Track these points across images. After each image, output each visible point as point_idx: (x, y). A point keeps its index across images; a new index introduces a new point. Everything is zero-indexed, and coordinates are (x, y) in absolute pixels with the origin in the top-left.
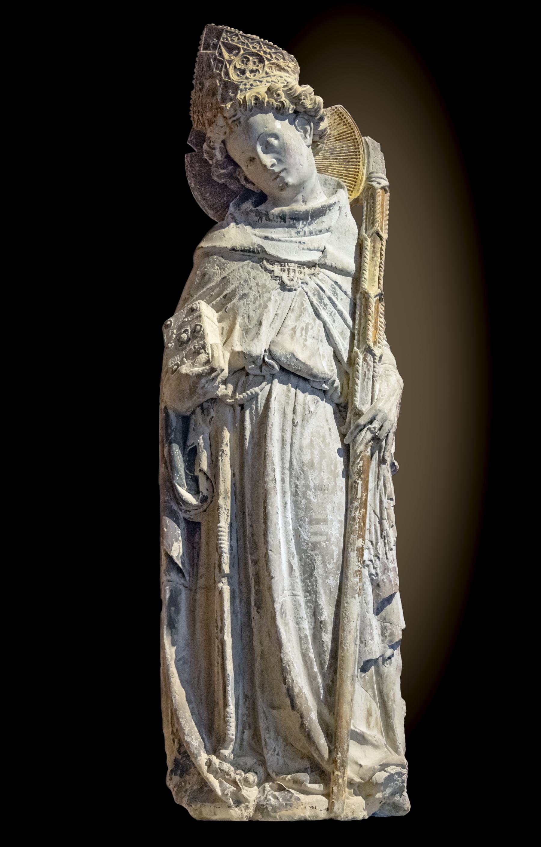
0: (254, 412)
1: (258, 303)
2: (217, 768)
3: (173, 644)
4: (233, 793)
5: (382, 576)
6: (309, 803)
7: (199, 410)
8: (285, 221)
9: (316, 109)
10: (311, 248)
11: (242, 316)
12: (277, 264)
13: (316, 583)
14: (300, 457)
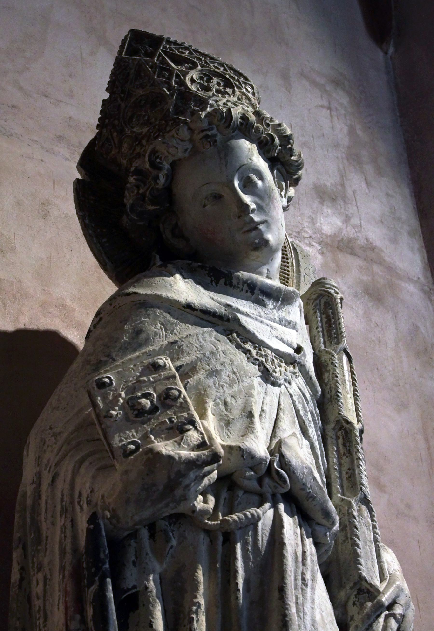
0: (250, 548)
1: (236, 388)
7: (145, 533)
8: (253, 293)
9: (300, 165)
10: (285, 339)
12: (251, 344)
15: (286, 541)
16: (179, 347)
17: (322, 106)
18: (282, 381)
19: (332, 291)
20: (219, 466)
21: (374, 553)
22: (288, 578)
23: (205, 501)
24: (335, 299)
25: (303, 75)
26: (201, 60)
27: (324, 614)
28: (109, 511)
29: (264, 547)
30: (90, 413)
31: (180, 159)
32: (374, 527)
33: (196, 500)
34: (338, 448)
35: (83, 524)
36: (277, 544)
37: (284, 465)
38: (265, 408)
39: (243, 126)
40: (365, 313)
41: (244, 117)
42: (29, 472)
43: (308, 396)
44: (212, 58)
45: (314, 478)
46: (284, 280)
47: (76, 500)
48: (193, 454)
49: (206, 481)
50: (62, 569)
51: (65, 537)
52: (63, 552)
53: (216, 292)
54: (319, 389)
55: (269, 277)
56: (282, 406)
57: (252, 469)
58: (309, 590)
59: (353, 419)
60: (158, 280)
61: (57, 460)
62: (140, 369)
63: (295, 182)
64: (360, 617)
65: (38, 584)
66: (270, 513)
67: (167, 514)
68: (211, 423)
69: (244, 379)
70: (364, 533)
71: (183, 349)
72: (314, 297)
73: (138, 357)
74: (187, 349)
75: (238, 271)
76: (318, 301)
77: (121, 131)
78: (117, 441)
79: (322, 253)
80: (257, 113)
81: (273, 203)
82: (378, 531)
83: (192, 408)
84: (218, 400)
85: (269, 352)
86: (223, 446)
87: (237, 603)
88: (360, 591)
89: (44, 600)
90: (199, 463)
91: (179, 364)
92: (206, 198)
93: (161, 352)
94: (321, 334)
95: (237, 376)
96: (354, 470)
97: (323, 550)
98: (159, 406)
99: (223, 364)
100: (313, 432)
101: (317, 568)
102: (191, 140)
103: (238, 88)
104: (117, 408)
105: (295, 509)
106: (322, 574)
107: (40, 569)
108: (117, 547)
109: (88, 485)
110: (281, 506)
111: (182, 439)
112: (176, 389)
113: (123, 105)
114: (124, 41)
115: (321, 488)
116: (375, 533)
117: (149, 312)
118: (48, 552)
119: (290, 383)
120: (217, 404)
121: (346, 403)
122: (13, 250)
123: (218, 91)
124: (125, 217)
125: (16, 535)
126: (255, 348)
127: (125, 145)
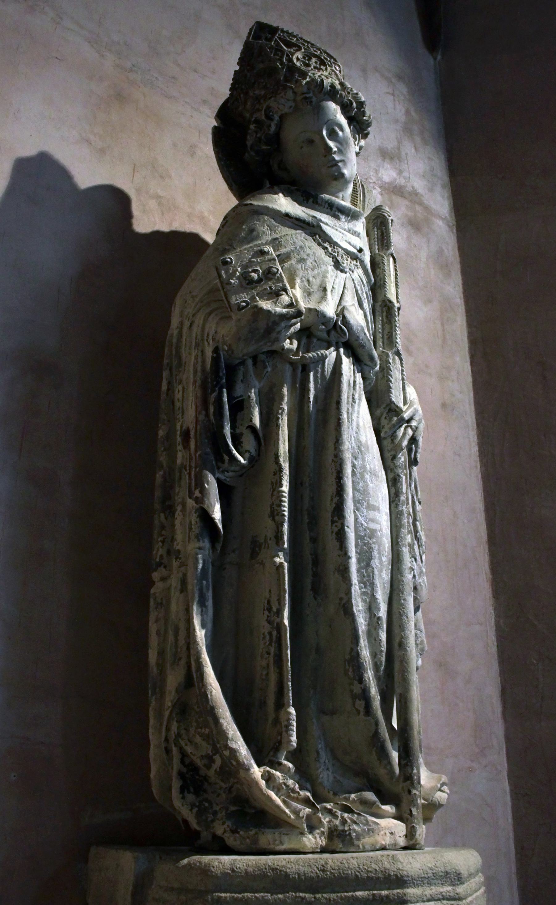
1: (316, 271)
2: (280, 784)
3: (203, 626)
4: (308, 817)
5: (419, 579)
6: (388, 829)
7: (250, 362)
8: (331, 209)
10: (352, 243)
11: (301, 279)
13: (373, 574)
14: (358, 436)
15: (343, 372)
16: (279, 242)
17: (388, 93)
18: (348, 270)
19: (386, 215)
20: (302, 320)
21: (401, 387)
22: (343, 396)
23: (291, 343)
24: (388, 220)
25: (376, 70)
26: (304, 45)
27: (365, 422)
28: (227, 346)
29: (329, 376)
30: (216, 284)
31: (286, 114)
32: (402, 371)
33: (285, 342)
34: (382, 318)
35: (209, 353)
36: (337, 375)
37: (345, 323)
38: (335, 287)
39: (332, 92)
40: (408, 237)
41: (332, 86)
42: (175, 321)
43: (365, 282)
44: (312, 44)
45: (365, 334)
46: (354, 201)
47: (205, 338)
48: (284, 311)
49: (292, 330)
50: (195, 382)
51: (197, 361)
52: (195, 372)
53: (307, 207)
54: (373, 279)
55: (344, 200)
56: (346, 286)
57: (323, 324)
58: (356, 406)
59: (394, 300)
60: (267, 196)
61: (194, 312)
62: (252, 253)
63: (365, 136)
64: (389, 426)
65: (179, 392)
66: (334, 354)
67: (265, 350)
68: (298, 292)
69: (322, 266)
70: (396, 375)
71: (281, 244)
72: (373, 218)
73: (251, 247)
74: (285, 244)
75: (322, 194)
76: (376, 221)
77: (246, 93)
78: (234, 300)
79: (382, 194)
80: (341, 84)
81: (349, 148)
82: (404, 373)
83: (285, 280)
84: (304, 279)
85: (340, 250)
86: (305, 308)
87: (309, 411)
88: (390, 410)
89: (183, 402)
90: (288, 317)
91: (278, 253)
92: (303, 142)
93: (266, 244)
94: (376, 243)
95: (317, 264)
96: (392, 333)
97: (368, 382)
98: (264, 278)
99: (308, 255)
100: (366, 305)
101: (363, 392)
102: (294, 100)
103: (329, 66)
104: (235, 278)
105: (351, 355)
106: (367, 399)
107: (180, 382)
108: (232, 370)
109: (213, 328)
110: (342, 350)
111: (278, 300)
112: (275, 268)
113: (249, 75)
114: (251, 30)
115: (369, 341)
116: (402, 374)
117: (260, 218)
118: (186, 372)
119: (353, 272)
120: (302, 281)
121: (390, 290)
122: (170, 177)
123: (315, 68)
124: (247, 154)
125: (166, 361)
126: (331, 246)
127: (249, 104)
